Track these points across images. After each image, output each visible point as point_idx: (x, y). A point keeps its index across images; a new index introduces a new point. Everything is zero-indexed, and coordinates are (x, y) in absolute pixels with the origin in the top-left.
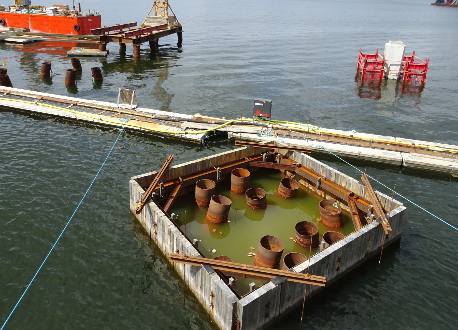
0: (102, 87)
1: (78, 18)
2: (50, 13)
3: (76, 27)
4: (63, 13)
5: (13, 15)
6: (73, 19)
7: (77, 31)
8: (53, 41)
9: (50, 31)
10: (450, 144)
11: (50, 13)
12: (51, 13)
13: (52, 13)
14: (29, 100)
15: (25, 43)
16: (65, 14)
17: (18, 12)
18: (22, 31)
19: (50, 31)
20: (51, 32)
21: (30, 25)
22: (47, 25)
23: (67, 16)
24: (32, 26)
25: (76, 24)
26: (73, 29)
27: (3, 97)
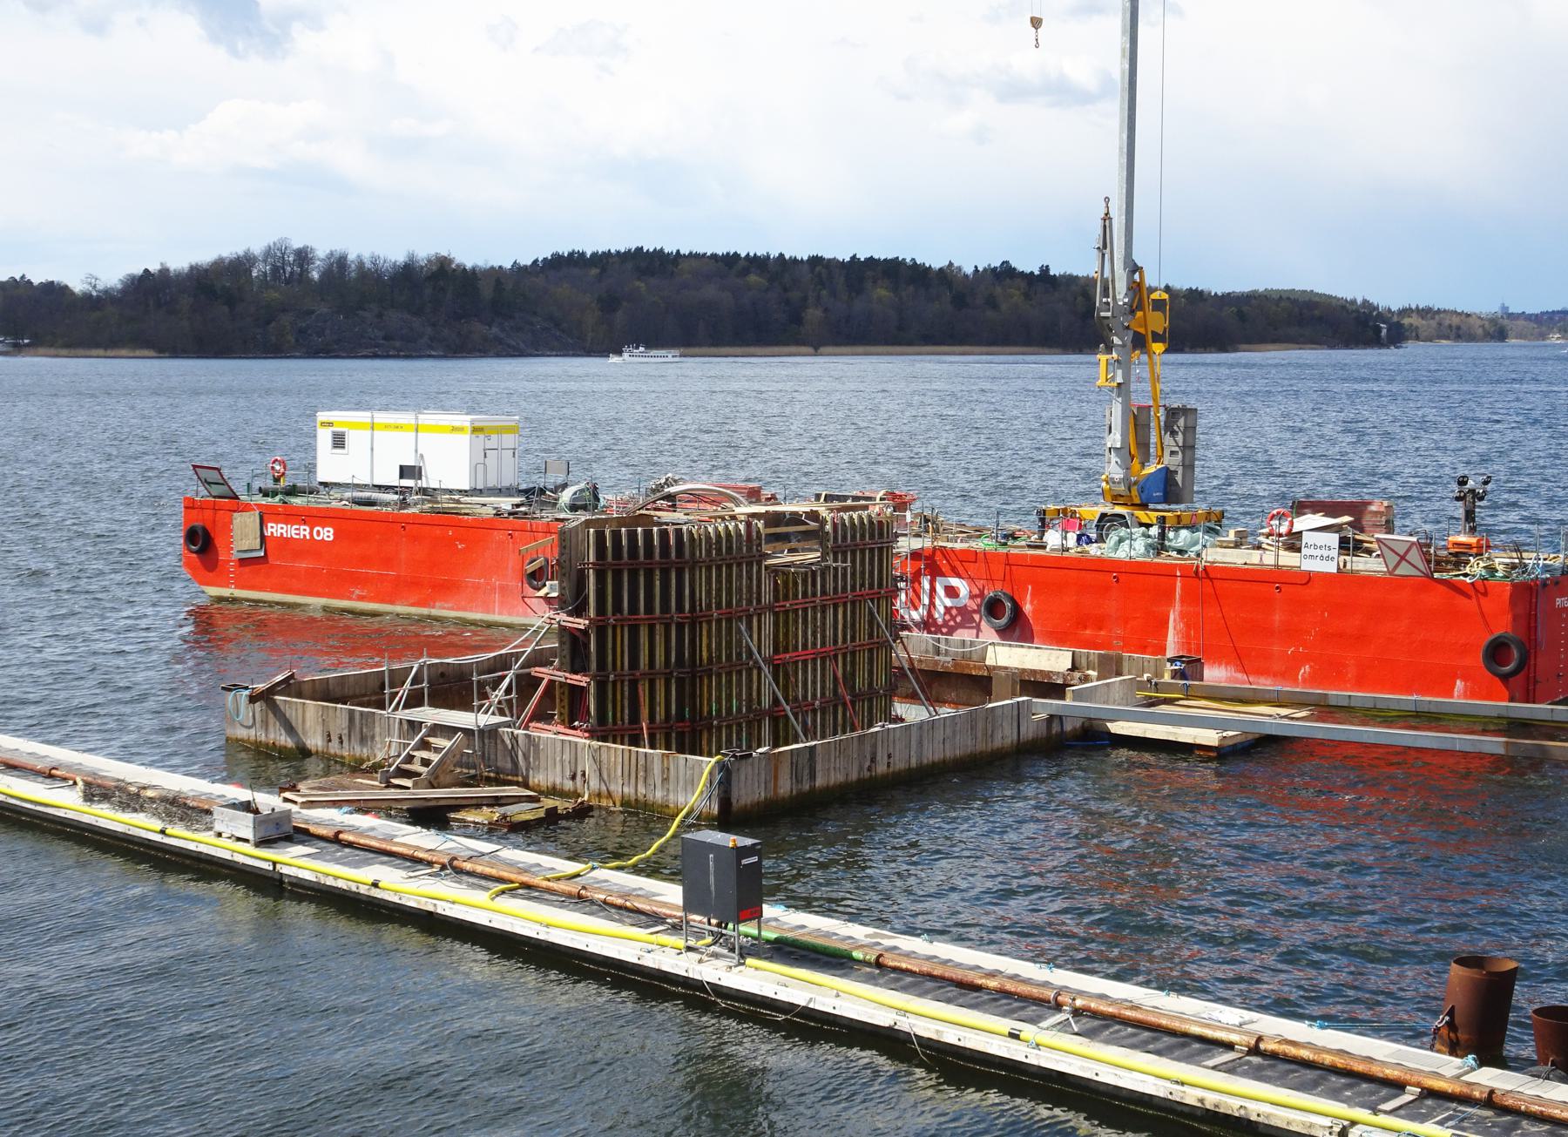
0: (641, 798)
1: (1515, 586)
2: (1318, 552)
3: (1496, 652)
4: (1415, 556)
5: (1062, 564)
6: (1485, 594)
7: (1505, 678)
8: (1365, 739)
9: (1305, 670)
10: (1062, 1076)
11: (1318, 552)
12: (1325, 553)
13: (1334, 553)
14: (1159, 1045)
15: (1221, 754)
16: (1429, 562)
17: (1093, 550)
18: (1167, 678)
19: (1305, 670)
20: (1312, 680)
21: (1177, 632)
22: (1291, 633)
23: (1436, 575)
24: (1188, 636)
25: (1503, 627)
26: (1477, 659)
27: (1402, 1112)
